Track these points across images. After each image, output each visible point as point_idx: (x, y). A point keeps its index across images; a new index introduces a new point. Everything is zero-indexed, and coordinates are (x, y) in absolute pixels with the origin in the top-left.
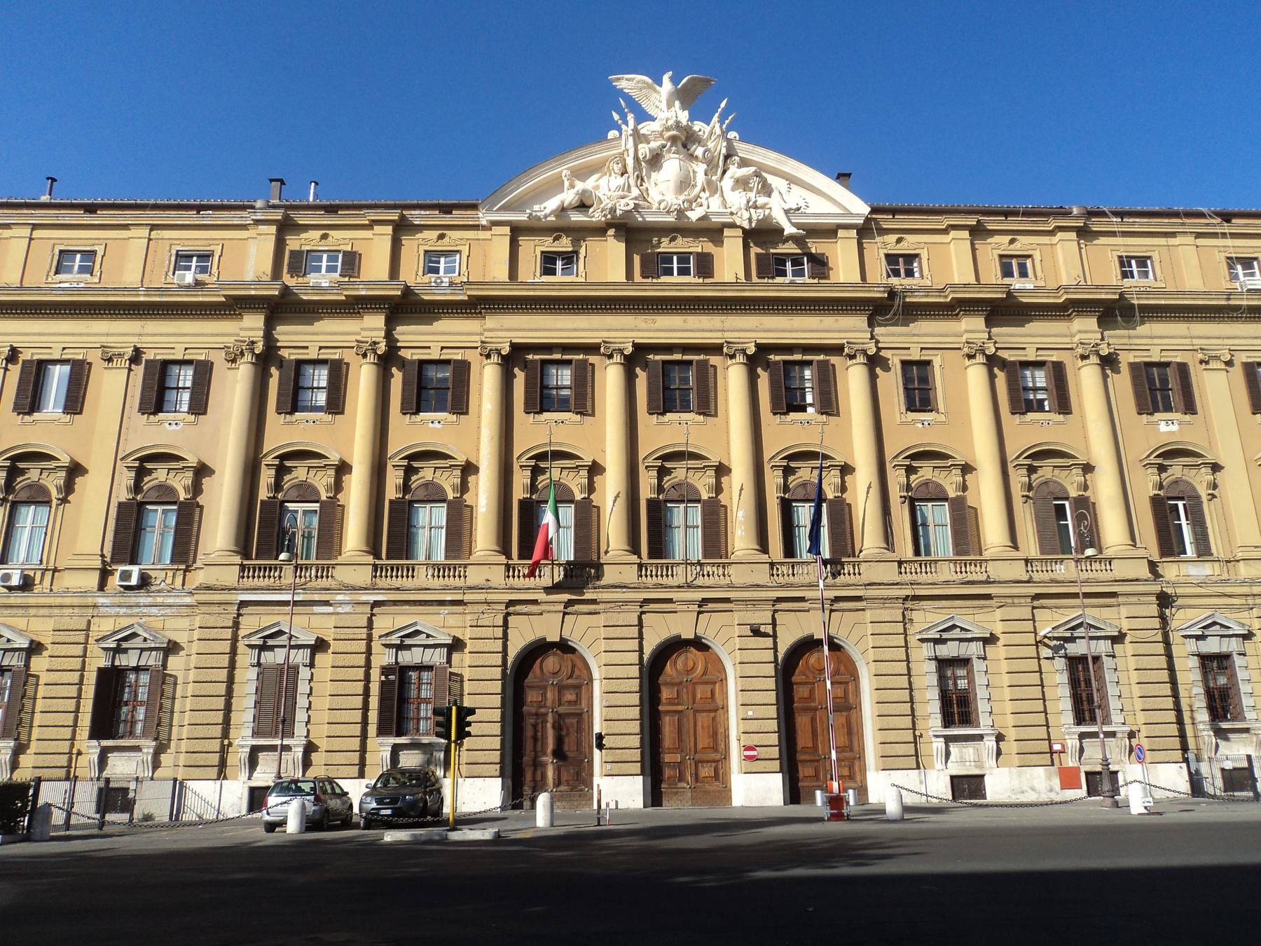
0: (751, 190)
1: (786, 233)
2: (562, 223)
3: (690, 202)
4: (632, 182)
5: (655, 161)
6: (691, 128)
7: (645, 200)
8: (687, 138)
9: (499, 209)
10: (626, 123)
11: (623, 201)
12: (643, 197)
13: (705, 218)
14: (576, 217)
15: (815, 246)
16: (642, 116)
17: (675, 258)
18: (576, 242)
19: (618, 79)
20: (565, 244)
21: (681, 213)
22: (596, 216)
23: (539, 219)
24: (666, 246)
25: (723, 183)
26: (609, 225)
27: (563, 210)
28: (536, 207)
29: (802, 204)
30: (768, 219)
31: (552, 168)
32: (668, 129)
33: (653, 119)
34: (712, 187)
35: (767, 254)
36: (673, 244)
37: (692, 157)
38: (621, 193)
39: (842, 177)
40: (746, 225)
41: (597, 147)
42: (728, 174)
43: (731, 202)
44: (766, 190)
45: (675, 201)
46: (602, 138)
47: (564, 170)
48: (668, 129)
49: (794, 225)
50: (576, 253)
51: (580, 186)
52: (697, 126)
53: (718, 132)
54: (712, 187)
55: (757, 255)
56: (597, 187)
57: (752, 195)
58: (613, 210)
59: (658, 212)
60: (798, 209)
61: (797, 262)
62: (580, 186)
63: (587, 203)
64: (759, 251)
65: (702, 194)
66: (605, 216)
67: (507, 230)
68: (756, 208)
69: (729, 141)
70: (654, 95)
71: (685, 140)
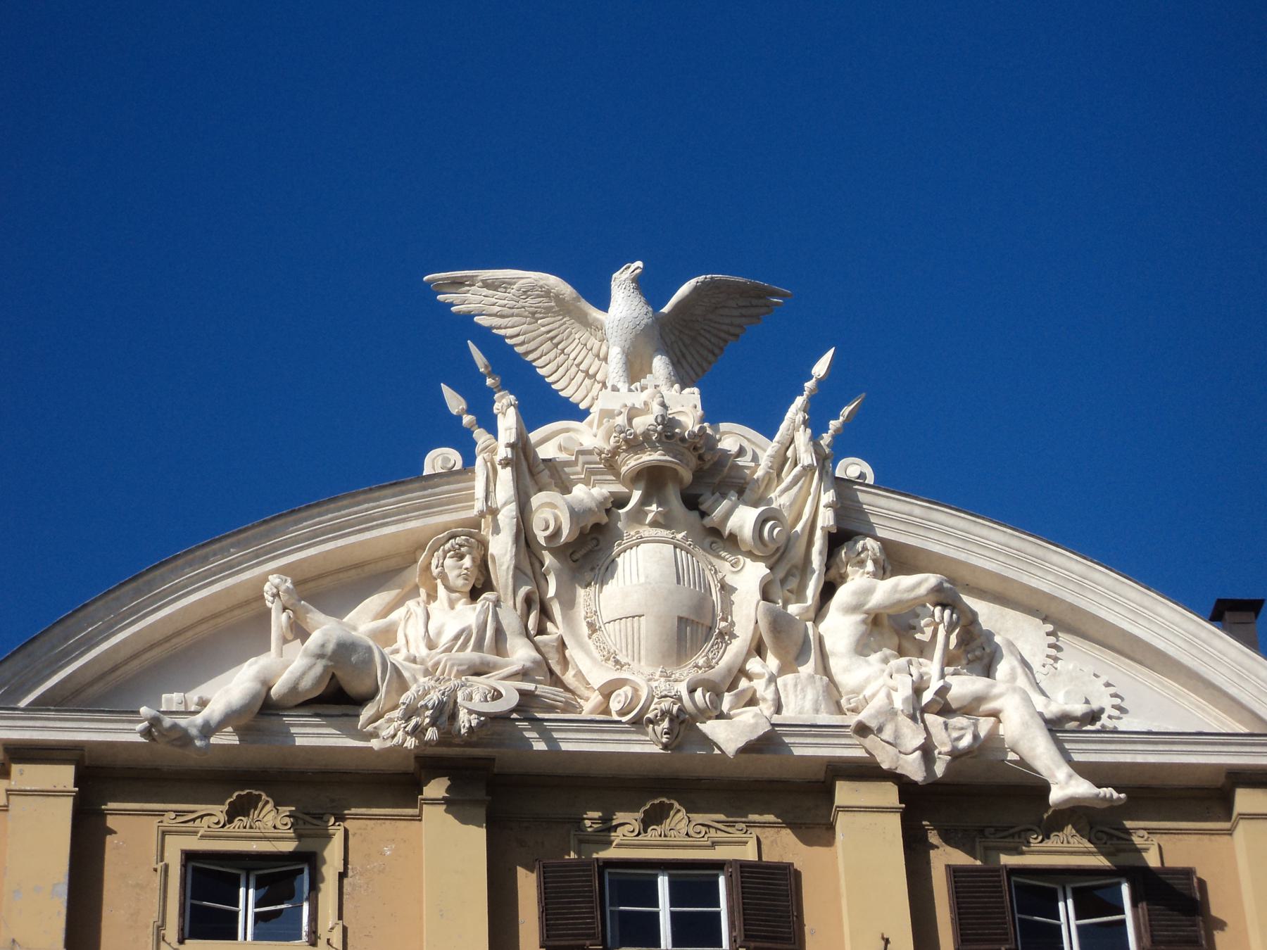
0: (923, 650)
1: (1056, 795)
2: (262, 754)
3: (716, 690)
4: (510, 619)
5: (590, 550)
6: (711, 443)
7: (556, 681)
8: (699, 475)
9: (42, 704)
10: (490, 425)
11: (480, 685)
12: (548, 669)
13: (768, 743)
14: (313, 735)
15: (1162, 846)
16: (544, 404)
17: (663, 883)
18: (311, 824)
19: (458, 284)
20: (269, 829)
21: (683, 725)
22: (386, 731)
23: (183, 738)
24: (628, 840)
25: (823, 627)
26: (429, 764)
27: (265, 710)
28: (170, 700)
29: (1102, 700)
30: (987, 748)
31: (231, 568)
32: (635, 445)
33: (579, 414)
34: (789, 641)
35: (992, 873)
36: (653, 833)
37: (719, 539)
38: (469, 654)
39: (1228, 612)
40: (913, 768)
41: (389, 502)
42: (843, 595)
43: (853, 687)
44: (977, 651)
45: (661, 685)
46: (404, 471)
47: (270, 576)
48: (635, 445)
49: (1084, 770)
50: (309, 860)
51: (325, 630)
52: (732, 437)
53: (807, 458)
54: (789, 641)
55: (955, 873)
56: (387, 635)
57: (932, 667)
58: (445, 712)
59: (602, 723)
60: (1094, 716)
61: (1094, 896)
62: (325, 630)
63: (355, 686)
64: (961, 858)
65: (754, 665)
66: (418, 731)
67: (64, 776)
68: (945, 710)
69: (842, 486)
70: (580, 334)
71: (691, 484)
